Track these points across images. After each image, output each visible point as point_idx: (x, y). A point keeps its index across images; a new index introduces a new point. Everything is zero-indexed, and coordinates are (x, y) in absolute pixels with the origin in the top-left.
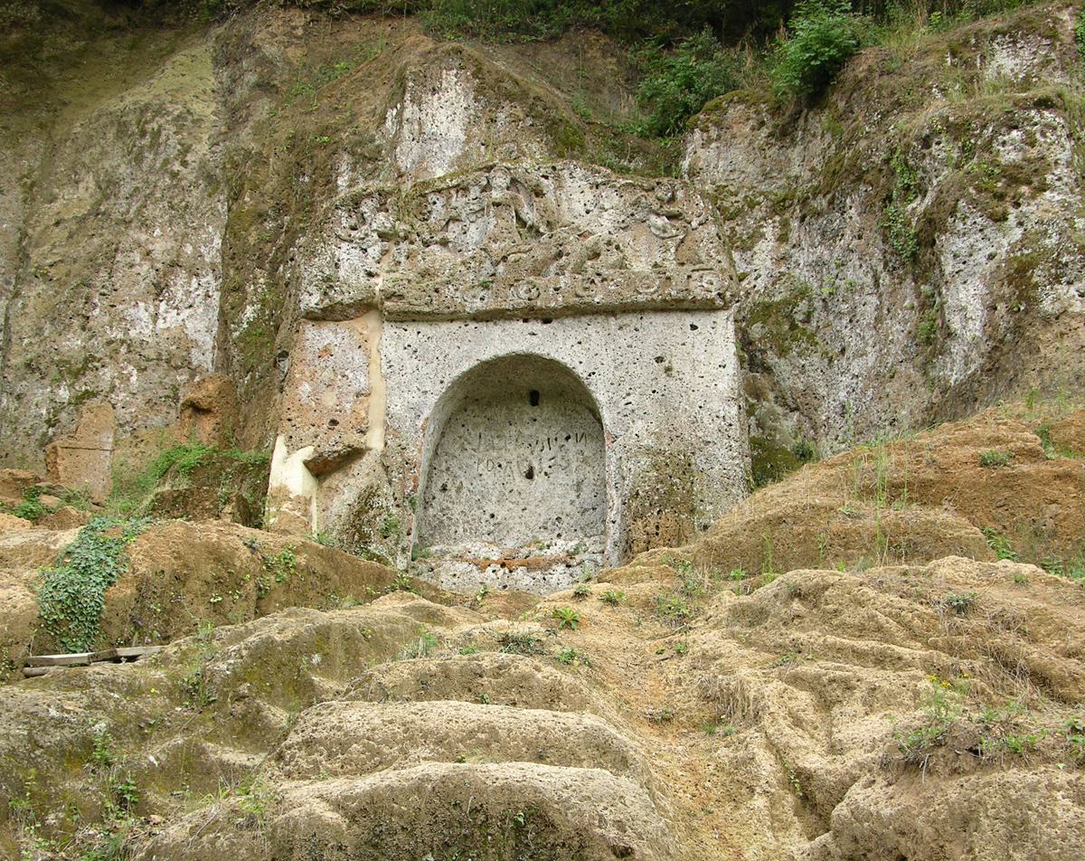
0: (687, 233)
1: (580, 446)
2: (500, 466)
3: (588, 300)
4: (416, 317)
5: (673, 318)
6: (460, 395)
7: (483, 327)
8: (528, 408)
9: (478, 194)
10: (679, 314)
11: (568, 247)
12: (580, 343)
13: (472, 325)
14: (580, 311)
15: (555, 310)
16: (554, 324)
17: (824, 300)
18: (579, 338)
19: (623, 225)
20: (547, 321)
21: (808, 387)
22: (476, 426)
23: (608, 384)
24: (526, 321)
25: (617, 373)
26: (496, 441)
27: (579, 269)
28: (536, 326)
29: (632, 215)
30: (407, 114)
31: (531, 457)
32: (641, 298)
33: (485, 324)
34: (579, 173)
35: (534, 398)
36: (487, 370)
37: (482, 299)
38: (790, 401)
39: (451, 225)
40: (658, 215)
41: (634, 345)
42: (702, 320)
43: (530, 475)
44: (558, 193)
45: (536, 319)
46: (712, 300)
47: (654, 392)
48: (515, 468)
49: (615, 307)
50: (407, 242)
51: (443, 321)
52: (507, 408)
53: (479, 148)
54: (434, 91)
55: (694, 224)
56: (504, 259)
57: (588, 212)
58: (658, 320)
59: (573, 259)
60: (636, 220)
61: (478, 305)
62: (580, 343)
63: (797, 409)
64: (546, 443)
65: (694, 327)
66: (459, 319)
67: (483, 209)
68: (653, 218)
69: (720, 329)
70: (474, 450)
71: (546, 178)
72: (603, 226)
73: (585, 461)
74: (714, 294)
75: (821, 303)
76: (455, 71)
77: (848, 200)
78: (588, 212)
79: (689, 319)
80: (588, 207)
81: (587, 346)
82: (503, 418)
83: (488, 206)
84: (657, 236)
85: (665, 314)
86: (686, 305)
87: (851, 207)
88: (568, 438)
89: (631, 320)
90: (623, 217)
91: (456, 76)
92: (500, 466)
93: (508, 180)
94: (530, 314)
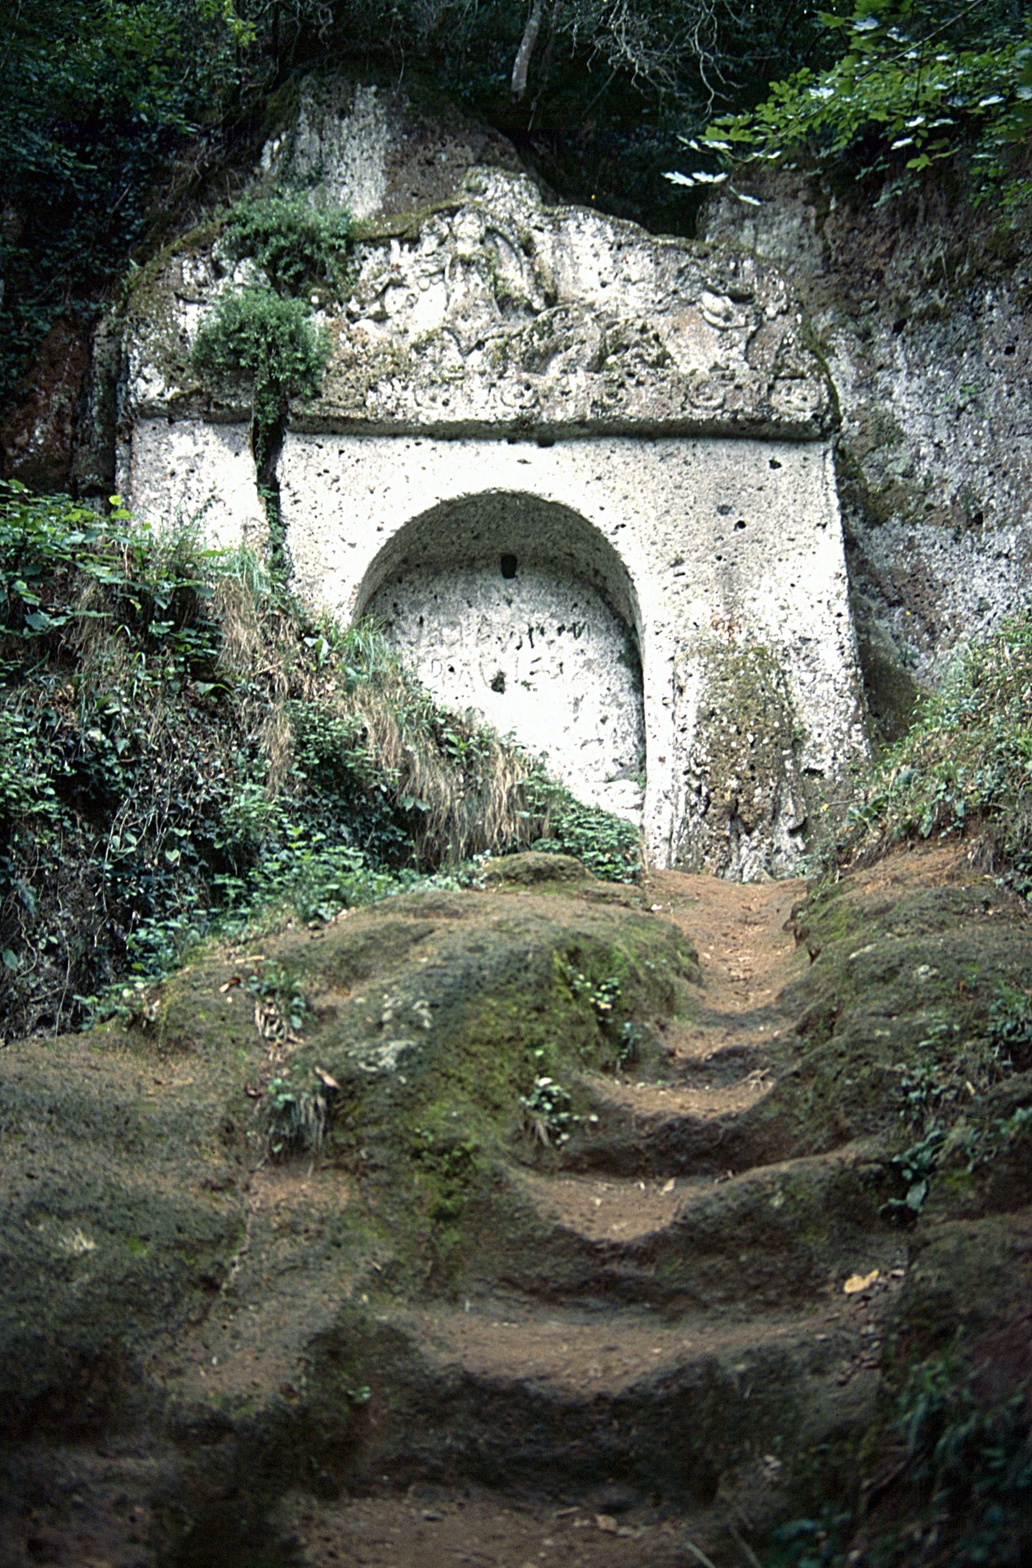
0: (760, 324)
1: (580, 643)
2: (452, 670)
3: (616, 412)
4: (339, 426)
5: (745, 449)
6: (397, 558)
7: (442, 446)
8: (499, 582)
9: (434, 247)
10: (752, 444)
11: (582, 331)
12: (599, 478)
13: (428, 444)
14: (598, 429)
15: (562, 424)
16: (558, 448)
17: (937, 445)
18: (599, 471)
19: (659, 307)
20: (545, 442)
21: (917, 569)
22: (417, 605)
23: (647, 544)
24: (512, 441)
25: (662, 528)
26: (446, 631)
27: (598, 364)
28: (527, 450)
29: (675, 292)
30: (302, 143)
31: (500, 656)
32: (700, 415)
33: (447, 444)
34: (591, 224)
35: (509, 567)
36: (449, 515)
37: (445, 404)
38: (890, 591)
39: (391, 291)
40: (717, 294)
41: (685, 484)
42: (788, 457)
43: (498, 684)
44: (558, 253)
45: (528, 439)
46: (806, 425)
47: (719, 558)
48: (476, 674)
49: (657, 426)
50: (323, 312)
51: (380, 435)
52: (467, 581)
53: (409, 200)
54: (342, 114)
55: (771, 311)
56: (480, 345)
57: (604, 285)
58: (721, 449)
59: (589, 352)
60: (682, 300)
61: (443, 415)
62: (599, 478)
63: (899, 603)
64: (526, 638)
65: (775, 465)
66: (408, 433)
67: (443, 272)
68: (707, 298)
69: (815, 472)
70: (411, 644)
71: (541, 230)
72: (632, 303)
73: (588, 664)
74: (809, 415)
75: (932, 448)
76: (374, 89)
77: (988, 298)
78: (604, 285)
79: (768, 453)
80: (605, 277)
81: (611, 483)
82: (458, 597)
83: (452, 265)
84: (714, 326)
85: (729, 443)
86: (765, 429)
87: (991, 308)
88: (560, 630)
89: (683, 449)
90: (660, 295)
91: (376, 94)
92: (452, 670)
93: (483, 230)
94: (524, 430)
